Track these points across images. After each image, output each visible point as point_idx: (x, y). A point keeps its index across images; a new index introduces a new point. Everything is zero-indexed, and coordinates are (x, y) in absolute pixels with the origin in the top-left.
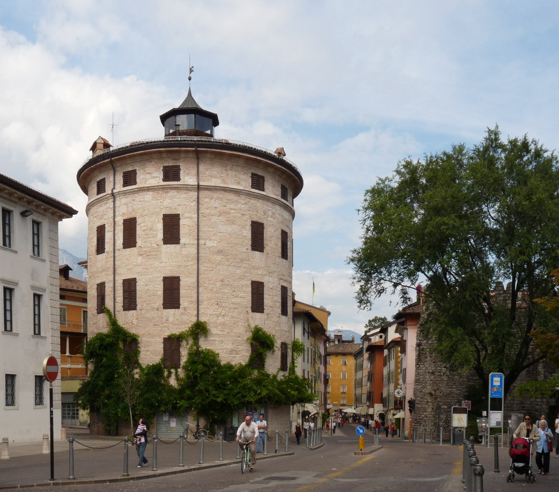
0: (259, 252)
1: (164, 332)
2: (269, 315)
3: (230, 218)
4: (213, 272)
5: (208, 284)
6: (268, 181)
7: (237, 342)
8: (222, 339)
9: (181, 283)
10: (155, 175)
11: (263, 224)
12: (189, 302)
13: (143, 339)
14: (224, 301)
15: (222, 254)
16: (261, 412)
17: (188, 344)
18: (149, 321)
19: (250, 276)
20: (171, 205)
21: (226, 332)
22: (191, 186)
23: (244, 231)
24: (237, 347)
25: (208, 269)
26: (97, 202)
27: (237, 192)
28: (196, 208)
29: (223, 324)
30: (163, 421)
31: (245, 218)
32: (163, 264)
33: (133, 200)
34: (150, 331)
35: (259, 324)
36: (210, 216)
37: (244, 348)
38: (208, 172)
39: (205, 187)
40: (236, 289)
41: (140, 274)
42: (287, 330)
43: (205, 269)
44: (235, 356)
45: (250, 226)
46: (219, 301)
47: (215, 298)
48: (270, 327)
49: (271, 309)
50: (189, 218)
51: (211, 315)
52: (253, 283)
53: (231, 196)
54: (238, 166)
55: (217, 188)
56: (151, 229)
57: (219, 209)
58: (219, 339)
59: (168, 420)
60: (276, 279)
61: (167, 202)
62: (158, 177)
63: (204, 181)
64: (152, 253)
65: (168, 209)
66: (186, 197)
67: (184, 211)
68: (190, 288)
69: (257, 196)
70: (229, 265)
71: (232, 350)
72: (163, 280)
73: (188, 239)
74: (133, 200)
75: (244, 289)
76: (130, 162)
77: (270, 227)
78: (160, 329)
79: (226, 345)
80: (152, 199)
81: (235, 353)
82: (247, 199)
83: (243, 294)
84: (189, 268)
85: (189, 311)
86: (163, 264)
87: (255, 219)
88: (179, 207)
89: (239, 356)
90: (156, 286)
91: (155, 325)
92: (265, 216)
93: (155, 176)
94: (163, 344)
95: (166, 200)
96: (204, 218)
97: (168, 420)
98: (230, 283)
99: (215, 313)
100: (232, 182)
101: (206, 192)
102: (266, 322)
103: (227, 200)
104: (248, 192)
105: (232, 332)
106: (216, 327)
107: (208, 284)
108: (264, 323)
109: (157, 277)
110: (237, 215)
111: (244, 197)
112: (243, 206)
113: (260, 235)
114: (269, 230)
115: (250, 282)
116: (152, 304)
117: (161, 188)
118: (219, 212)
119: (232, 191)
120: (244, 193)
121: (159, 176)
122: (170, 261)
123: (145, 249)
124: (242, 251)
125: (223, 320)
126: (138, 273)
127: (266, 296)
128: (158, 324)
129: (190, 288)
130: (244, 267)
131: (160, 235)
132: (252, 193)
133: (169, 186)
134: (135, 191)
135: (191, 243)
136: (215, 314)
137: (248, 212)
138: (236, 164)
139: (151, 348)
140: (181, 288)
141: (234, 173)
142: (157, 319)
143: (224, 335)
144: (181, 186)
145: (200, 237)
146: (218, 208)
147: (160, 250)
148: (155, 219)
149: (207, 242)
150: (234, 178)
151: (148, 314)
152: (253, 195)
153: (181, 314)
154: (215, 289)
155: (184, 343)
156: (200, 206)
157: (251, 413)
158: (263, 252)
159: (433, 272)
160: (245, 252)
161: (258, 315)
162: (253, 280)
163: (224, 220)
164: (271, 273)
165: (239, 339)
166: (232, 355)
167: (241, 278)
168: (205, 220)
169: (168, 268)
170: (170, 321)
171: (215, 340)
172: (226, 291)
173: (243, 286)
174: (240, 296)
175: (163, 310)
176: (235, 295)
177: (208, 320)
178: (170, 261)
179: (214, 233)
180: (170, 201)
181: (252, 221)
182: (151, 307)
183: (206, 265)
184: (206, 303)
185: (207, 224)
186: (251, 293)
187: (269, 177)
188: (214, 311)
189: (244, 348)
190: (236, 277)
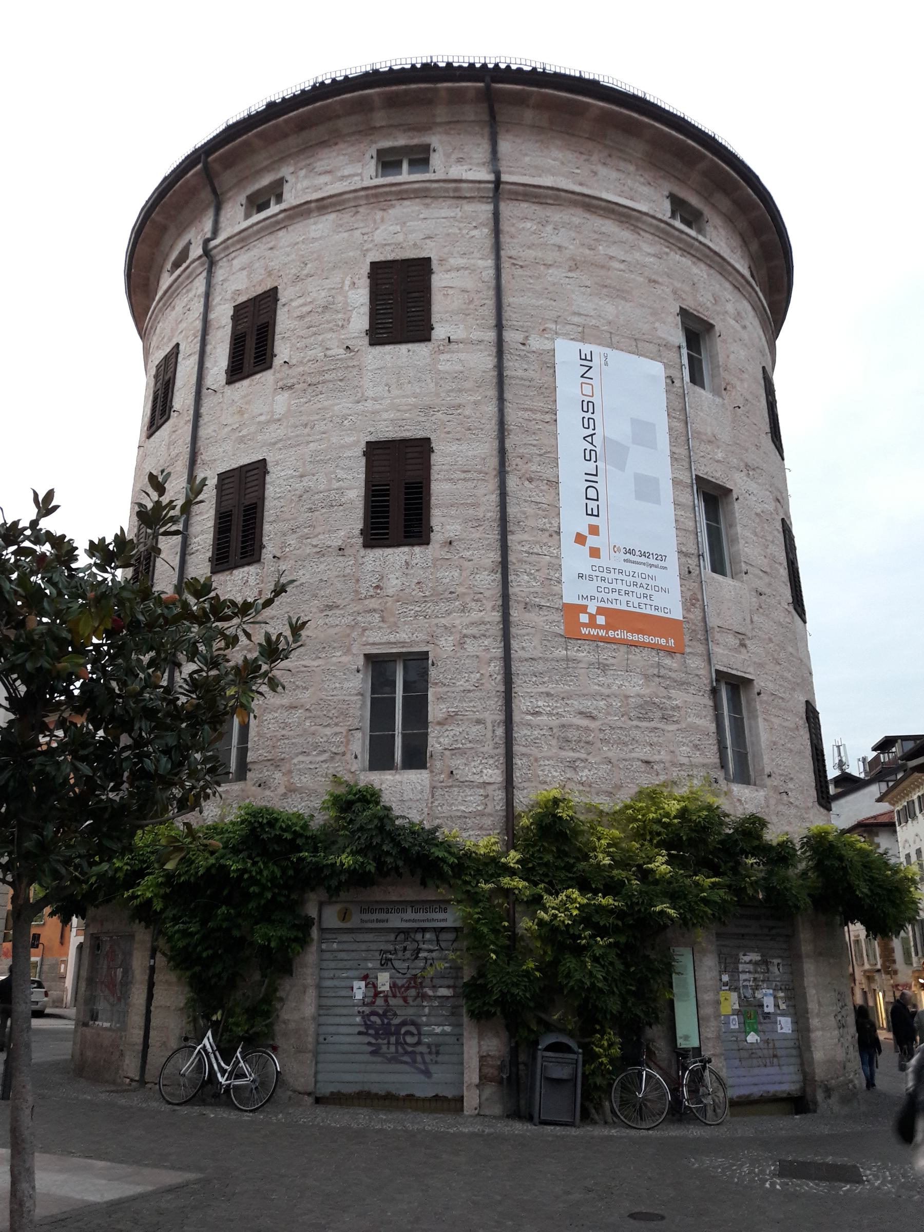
1: (364, 630)
9: (435, 458)
18: (306, 597)
20: (400, 238)
28: (489, 243)
36: (542, 267)
41: (279, 445)
55: (563, 194)
61: (386, 230)
62: (357, 175)
65: (388, 248)
67: (446, 250)
68: (469, 475)
72: (365, 454)
73: (462, 326)
74: (271, 249)
78: (348, 620)
84: (467, 413)
85: (467, 554)
86: (369, 404)
88: (428, 241)
90: (341, 474)
91: (330, 608)
101: (524, 205)
102: (755, 618)
109: (342, 447)
116: (321, 537)
119: (613, 211)
122: (395, 392)
123: (301, 369)
126: (275, 443)
128: (339, 602)
129: (469, 475)
131: (360, 321)
134: (278, 222)
139: (308, 694)
140: (434, 476)
142: (339, 586)
146: (566, 248)
147: (355, 363)
151: (301, 573)
152: (680, 240)
153: (435, 566)
156: (504, 239)
159: (163, 911)
163: (588, 283)
168: (521, 276)
169: (385, 415)
170: (391, 591)
175: (363, 552)
178: (395, 392)
189: (690, 698)
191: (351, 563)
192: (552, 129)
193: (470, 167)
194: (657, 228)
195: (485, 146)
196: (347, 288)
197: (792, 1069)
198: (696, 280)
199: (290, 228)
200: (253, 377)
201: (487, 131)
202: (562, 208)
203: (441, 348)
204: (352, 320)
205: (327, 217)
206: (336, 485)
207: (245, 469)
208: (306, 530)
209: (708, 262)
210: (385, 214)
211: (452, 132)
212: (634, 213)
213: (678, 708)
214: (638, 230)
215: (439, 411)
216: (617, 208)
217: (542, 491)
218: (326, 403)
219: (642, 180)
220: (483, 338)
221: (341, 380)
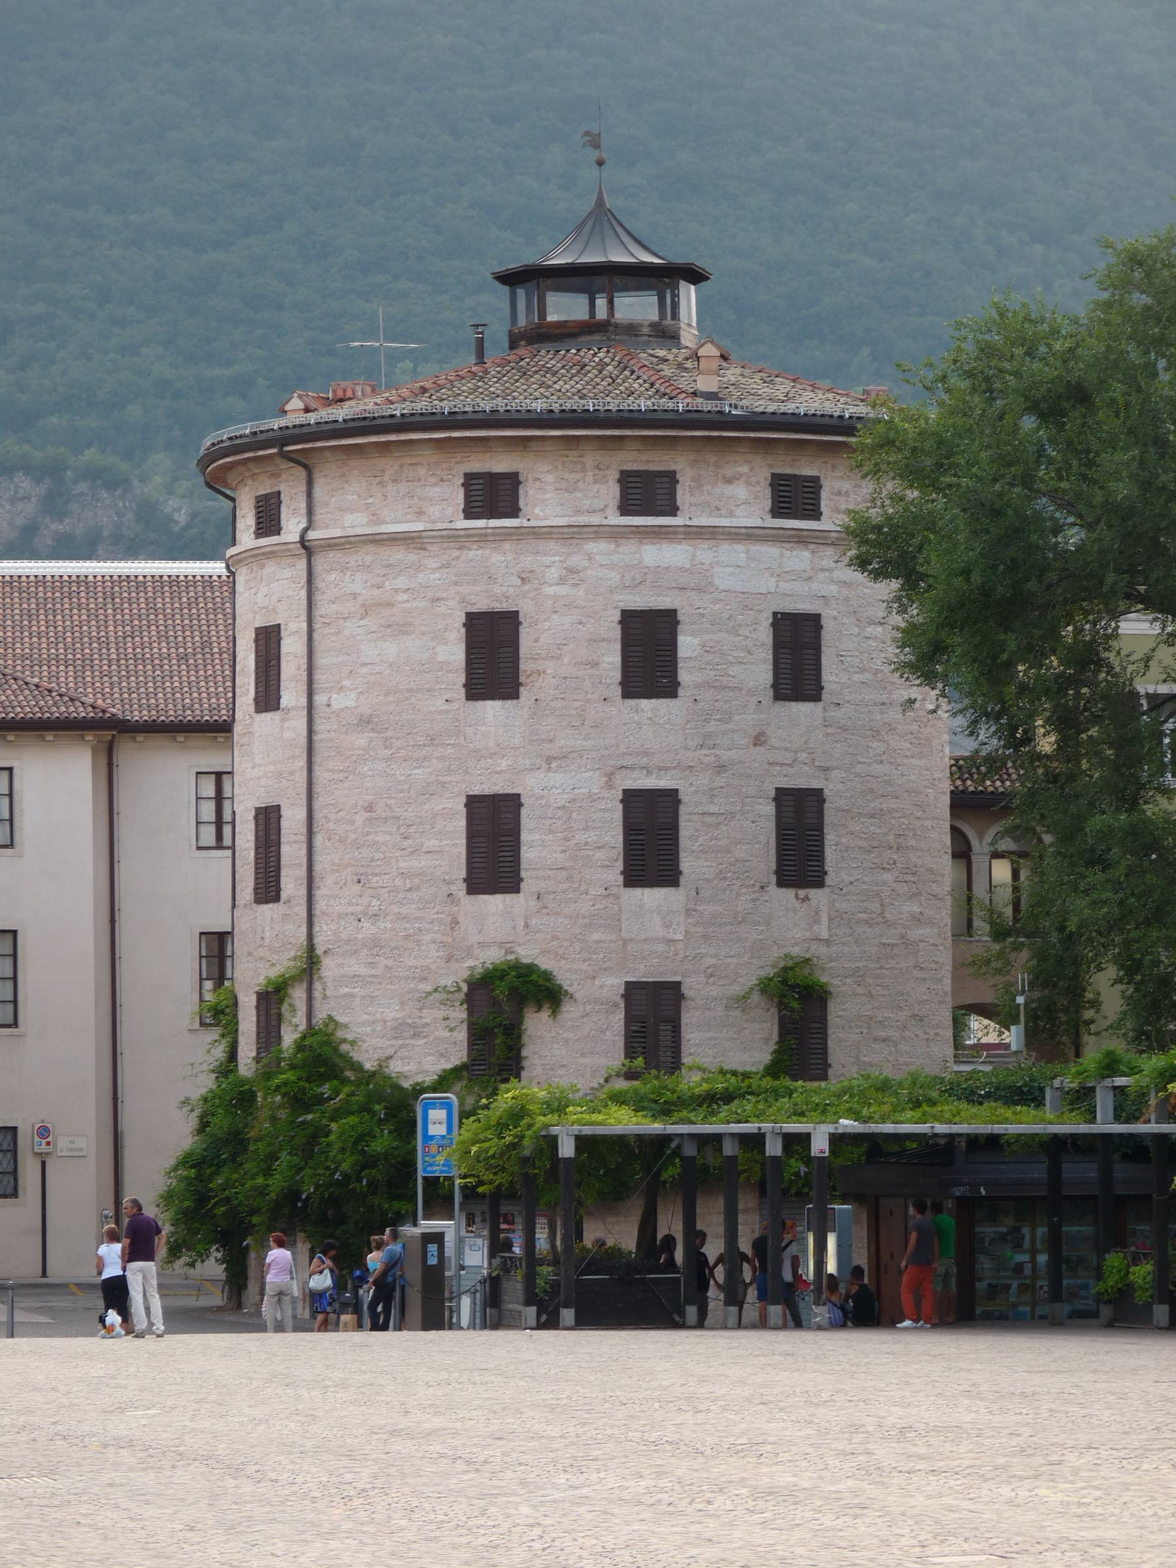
3: (393, 619)
14: (377, 871)
15: (371, 726)
26: (387, 540)
29: (374, 944)
31: (442, 609)
36: (341, 622)
38: (334, 499)
39: (323, 542)
40: (412, 830)
45: (463, 630)
49: (562, 875)
51: (341, 916)
52: (474, 803)
53: (397, 555)
54: (416, 464)
55: (352, 539)
63: (327, 527)
69: (486, 535)
70: (389, 759)
71: (401, 1024)
82: (449, 552)
87: (482, 605)
89: (424, 1041)
92: (527, 587)
96: (327, 630)
98: (393, 811)
99: (351, 909)
102: (533, 922)
104: (444, 533)
105: (400, 967)
106: (356, 952)
107: (337, 821)
108: (526, 926)
110: (415, 604)
112: (437, 575)
118: (363, 605)
119: (395, 539)
120: (434, 537)
124: (434, 709)
125: (374, 930)
130: (441, 758)
132: (462, 533)
136: (353, 914)
138: (408, 460)
143: (375, 976)
145: (315, 686)
146: (359, 594)
150: (407, 500)
156: (318, 597)
158: (515, 695)
162: (476, 793)
168: (327, 635)
171: (352, 996)
172: (380, 838)
174: (424, 849)
176: (411, 847)
181: (468, 614)
185: (333, 644)
186: (464, 835)
188: (350, 904)
194: (442, 537)
197: (1108, 1263)
213: (427, 1024)
214: (424, 546)
217: (336, 848)
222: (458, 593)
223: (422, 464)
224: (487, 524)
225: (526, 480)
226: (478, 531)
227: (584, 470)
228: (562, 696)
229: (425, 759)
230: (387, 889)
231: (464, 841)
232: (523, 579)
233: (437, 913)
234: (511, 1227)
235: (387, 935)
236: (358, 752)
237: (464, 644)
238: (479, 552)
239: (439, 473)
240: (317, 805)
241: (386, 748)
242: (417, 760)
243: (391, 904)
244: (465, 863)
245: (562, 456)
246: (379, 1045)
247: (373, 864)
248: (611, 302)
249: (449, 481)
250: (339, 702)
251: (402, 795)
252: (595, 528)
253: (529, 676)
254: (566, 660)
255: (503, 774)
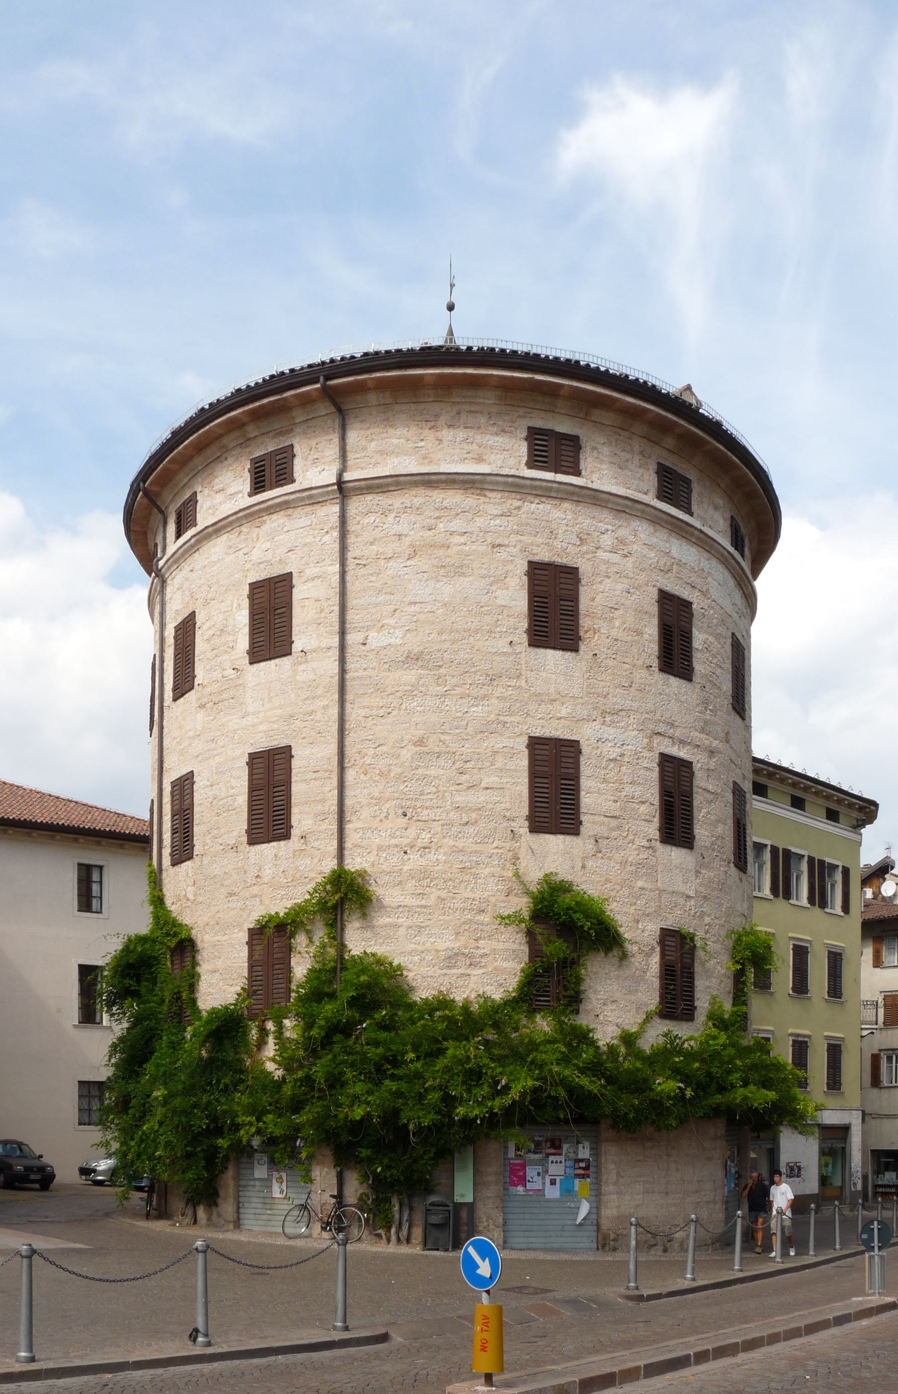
0: (559, 653)
2: (603, 843)
3: (448, 560)
4: (389, 719)
5: (375, 756)
6: (594, 448)
7: (474, 926)
8: (417, 920)
9: (295, 763)
10: (232, 490)
11: (577, 569)
12: (316, 815)
13: (207, 937)
14: (428, 804)
15: (420, 663)
16: (576, 1153)
17: (311, 941)
19: (524, 723)
20: (269, 555)
21: (433, 897)
22: (320, 490)
23: (499, 593)
24: (475, 944)
25: (374, 712)
27: (473, 482)
29: (424, 875)
30: (255, 1180)
32: (250, 720)
33: (192, 571)
34: (219, 915)
35: (560, 870)
36: (382, 562)
37: (501, 946)
38: (373, 444)
39: (363, 483)
40: (468, 765)
42: (692, 894)
43: (364, 714)
44: (468, 971)
45: (525, 579)
46: (409, 803)
47: (396, 795)
48: (608, 880)
49: (614, 823)
50: (318, 577)
51: (380, 848)
52: (536, 744)
53: (452, 498)
55: (402, 479)
56: (222, 630)
57: (409, 539)
58: (409, 922)
59: (266, 1177)
60: (635, 733)
64: (225, 696)
65: (262, 566)
66: (309, 523)
69: (550, 489)
70: (445, 695)
71: (456, 955)
74: (192, 571)
75: (499, 764)
76: (186, 480)
77: (607, 581)
79: (432, 940)
80: (226, 554)
81: (468, 962)
82: (510, 501)
83: (496, 779)
84: (317, 718)
85: (316, 844)
86: (250, 718)
87: (544, 555)
88: (290, 554)
89: (481, 971)
92: (585, 548)
93: (233, 492)
94: (247, 946)
95: (258, 546)
96: (363, 571)
97: (266, 1177)
99: (394, 841)
100: (456, 458)
101: (369, 497)
102: (590, 864)
103: (437, 509)
105: (454, 898)
108: (583, 867)
111: (499, 496)
112: (498, 522)
113: (562, 603)
114: (601, 587)
115: (525, 740)
116: (224, 837)
117: (246, 516)
118: (411, 546)
119: (454, 482)
120: (497, 483)
121: (240, 489)
127: (585, 783)
131: (243, 643)
132: (529, 482)
133: (262, 506)
135: (323, 645)
136: (396, 846)
137: (514, 538)
138: (467, 407)
141: (461, 434)
142: (235, 877)
143: (425, 907)
144: (293, 497)
145: (348, 626)
148: (232, 602)
149: (373, 634)
150: (465, 446)
151: (215, 866)
153: (294, 855)
154: (396, 770)
155: (300, 940)
156: (351, 539)
157: (537, 1156)
158: (576, 650)
160: (505, 653)
161: (555, 843)
164: (610, 715)
165: (480, 918)
166: (455, 971)
167: (486, 730)
168: (363, 576)
170: (266, 879)
171: (397, 926)
172: (432, 772)
173: (495, 753)
174: (483, 785)
177: (373, 865)
179: (393, 607)
180: (269, 544)
181: (530, 562)
182: (221, 844)
183: (366, 701)
184: (365, 813)
185: (370, 584)
186: (526, 774)
187: (602, 440)
190: (470, 729)
191: (241, 858)
192: (396, 403)
193: (323, 467)
194: (506, 484)
195: (335, 438)
196: (234, 610)
198: (554, 526)
199: (201, 550)
200: (185, 696)
201: (337, 422)
202: (404, 491)
203: (299, 659)
204: (239, 641)
205: (221, 538)
206: (232, 792)
207: (183, 780)
208: (215, 831)
209: (575, 498)
210: (259, 529)
211: (309, 431)
212: (476, 477)
215: (297, 719)
216: (457, 477)
217: (375, 781)
218: (224, 720)
219: (495, 429)
220: (330, 645)
221: (233, 698)
222: (521, 541)
223: (482, 413)
224: (555, 477)
225: (586, 447)
226: (544, 484)
227: (632, 451)
228: (614, 656)
229: (484, 697)
230: (441, 822)
231: (526, 780)
232: (581, 539)
233: (497, 847)
234: (557, 1151)
235: (440, 867)
236: (406, 688)
237: (526, 591)
238: (541, 506)
239: (500, 423)
240: (348, 741)
241: (439, 685)
242: (476, 698)
243: (444, 837)
244: (527, 801)
245: (616, 433)
246: (430, 974)
247: (422, 797)
248: (337, 503)
249: (511, 432)
250: (376, 639)
251: (458, 731)
252: (644, 507)
253: (586, 632)
254: (617, 624)
255: (563, 721)
